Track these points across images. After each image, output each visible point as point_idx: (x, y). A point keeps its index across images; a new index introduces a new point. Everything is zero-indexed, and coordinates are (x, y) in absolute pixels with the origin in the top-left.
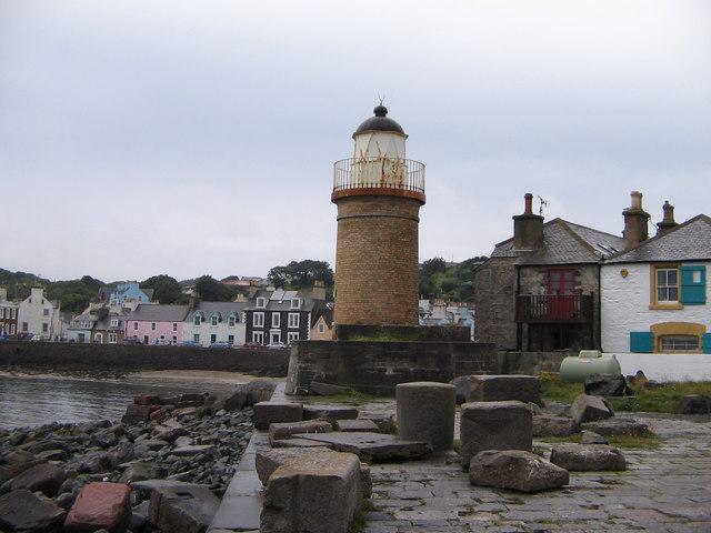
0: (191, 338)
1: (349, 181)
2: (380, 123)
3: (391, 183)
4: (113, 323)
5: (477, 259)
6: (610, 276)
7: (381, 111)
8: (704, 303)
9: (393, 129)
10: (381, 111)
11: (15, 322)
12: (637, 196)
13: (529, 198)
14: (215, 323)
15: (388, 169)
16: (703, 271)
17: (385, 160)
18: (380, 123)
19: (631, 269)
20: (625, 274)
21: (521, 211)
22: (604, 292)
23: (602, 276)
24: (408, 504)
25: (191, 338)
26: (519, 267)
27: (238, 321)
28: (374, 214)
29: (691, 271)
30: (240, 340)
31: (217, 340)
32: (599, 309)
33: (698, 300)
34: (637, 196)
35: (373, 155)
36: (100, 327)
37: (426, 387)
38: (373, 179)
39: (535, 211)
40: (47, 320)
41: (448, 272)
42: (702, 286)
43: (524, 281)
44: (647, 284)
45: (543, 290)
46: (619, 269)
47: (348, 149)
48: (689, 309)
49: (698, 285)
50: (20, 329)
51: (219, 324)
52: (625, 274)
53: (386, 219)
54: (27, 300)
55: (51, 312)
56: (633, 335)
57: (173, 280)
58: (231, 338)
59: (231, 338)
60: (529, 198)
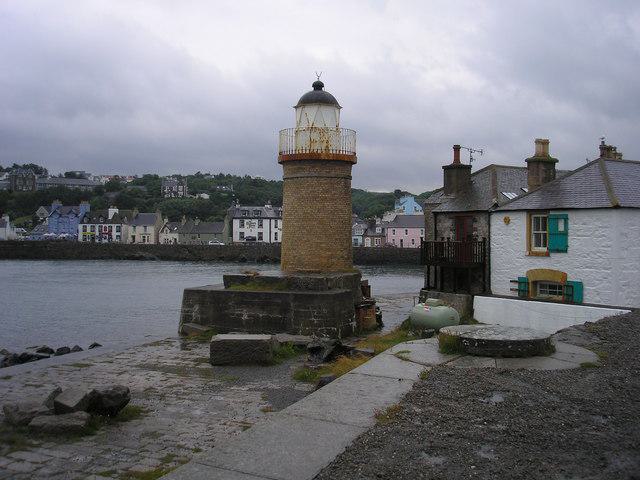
1: (293, 146)
2: (318, 97)
3: (318, 148)
4: (378, 230)
6: (497, 221)
7: (318, 86)
8: (566, 251)
10: (318, 86)
13: (457, 149)
16: (566, 220)
17: (312, 129)
18: (318, 97)
19: (512, 216)
21: (450, 160)
22: (493, 237)
23: (492, 224)
24: (209, 463)
28: (298, 175)
29: (557, 218)
35: (304, 126)
36: (370, 233)
39: (464, 160)
42: (565, 234)
44: (523, 231)
46: (502, 217)
47: (291, 118)
48: (555, 257)
49: (561, 234)
52: (507, 221)
60: (457, 149)
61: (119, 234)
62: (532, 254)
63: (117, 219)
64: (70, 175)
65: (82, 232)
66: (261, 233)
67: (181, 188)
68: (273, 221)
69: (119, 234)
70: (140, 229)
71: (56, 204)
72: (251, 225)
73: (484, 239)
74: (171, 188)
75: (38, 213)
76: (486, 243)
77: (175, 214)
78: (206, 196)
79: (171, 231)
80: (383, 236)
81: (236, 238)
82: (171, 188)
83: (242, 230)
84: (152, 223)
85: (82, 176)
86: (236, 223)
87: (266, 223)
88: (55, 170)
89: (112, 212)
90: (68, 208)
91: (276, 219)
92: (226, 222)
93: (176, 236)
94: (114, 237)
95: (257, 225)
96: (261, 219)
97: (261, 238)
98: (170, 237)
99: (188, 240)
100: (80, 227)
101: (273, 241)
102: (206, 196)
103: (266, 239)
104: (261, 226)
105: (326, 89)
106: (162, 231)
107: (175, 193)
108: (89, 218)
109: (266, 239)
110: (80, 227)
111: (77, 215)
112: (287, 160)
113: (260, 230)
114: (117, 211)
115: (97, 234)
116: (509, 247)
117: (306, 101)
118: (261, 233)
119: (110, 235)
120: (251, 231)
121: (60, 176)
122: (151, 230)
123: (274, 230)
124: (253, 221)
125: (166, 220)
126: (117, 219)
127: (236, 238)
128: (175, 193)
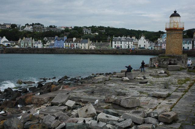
0: (187, 48)
1: (168, 27)
2: (175, 15)
3: (176, 27)
4: (159, 45)
7: (175, 12)
9: (178, 16)
10: (175, 12)
11: (137, 45)
12: (143, 61)
15: (175, 24)
18: (175, 15)
25: (187, 48)
27: (190, 43)
30: (191, 48)
34: (143, 61)
37: (171, 66)
38: (172, 27)
40: (145, 44)
50: (139, 46)
55: (146, 42)
58: (188, 47)
59: (188, 47)
61: (76, 46)
63: (76, 41)
64: (51, 27)
65: (66, 45)
66: (121, 46)
67: (89, 31)
68: (125, 42)
69: (76, 46)
70: (83, 44)
71: (56, 37)
72: (118, 43)
74: (86, 31)
75: (44, 39)
77: (94, 40)
78: (97, 34)
79: (93, 45)
80: (161, 47)
81: (113, 47)
82: (86, 31)
83: (115, 45)
84: (87, 43)
85: (55, 27)
86: (113, 42)
87: (123, 42)
88: (46, 25)
89: (74, 39)
90: (61, 38)
91: (126, 41)
92: (111, 42)
93: (95, 47)
94: (75, 47)
95: (120, 43)
96: (121, 41)
97: (121, 47)
98: (93, 47)
99: (98, 48)
100: (64, 44)
101: (125, 48)
102: (97, 34)
103: (123, 48)
104: (121, 43)
106: (90, 45)
107: (87, 33)
108: (67, 41)
109: (123, 48)
110: (64, 44)
111: (63, 40)
112: (167, 29)
113: (121, 45)
114: (75, 39)
115: (70, 46)
117: (172, 16)
118: (121, 46)
119: (74, 46)
120: (118, 44)
121: (48, 27)
122: (87, 45)
123: (125, 45)
124: (119, 42)
125: (91, 42)
126: (76, 41)
127: (113, 47)
128: (87, 33)
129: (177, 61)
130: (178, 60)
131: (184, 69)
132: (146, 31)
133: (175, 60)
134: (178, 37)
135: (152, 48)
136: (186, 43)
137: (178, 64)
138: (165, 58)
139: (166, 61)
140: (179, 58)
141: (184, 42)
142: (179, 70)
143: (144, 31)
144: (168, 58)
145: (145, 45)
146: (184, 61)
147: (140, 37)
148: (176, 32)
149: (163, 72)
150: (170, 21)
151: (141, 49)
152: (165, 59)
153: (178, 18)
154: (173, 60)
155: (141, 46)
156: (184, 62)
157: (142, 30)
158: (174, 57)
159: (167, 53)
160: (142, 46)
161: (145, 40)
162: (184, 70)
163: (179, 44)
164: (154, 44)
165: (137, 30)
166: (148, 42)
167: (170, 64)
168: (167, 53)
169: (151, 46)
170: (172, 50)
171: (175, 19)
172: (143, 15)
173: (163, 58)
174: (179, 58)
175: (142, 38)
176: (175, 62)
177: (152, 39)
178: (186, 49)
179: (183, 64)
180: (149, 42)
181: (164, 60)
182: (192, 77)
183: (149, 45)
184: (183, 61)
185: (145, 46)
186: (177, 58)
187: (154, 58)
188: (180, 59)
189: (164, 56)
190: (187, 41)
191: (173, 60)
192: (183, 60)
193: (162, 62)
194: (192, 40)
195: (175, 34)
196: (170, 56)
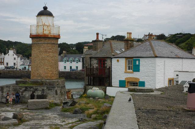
1: (34, 33)
2: (45, 12)
3: (46, 32)
5: (177, 34)
6: (114, 61)
7: (45, 8)
8: (139, 71)
9: (50, 14)
10: (45, 8)
11: (3, 62)
13: (98, 34)
14: (77, 62)
15: (45, 28)
16: (139, 61)
18: (45, 12)
19: (119, 59)
20: (118, 61)
21: (95, 39)
22: (113, 66)
26: (91, 58)
27: (79, 61)
29: (136, 60)
30: (80, 68)
31: (72, 68)
32: (111, 72)
33: (137, 70)
38: (40, 32)
40: (15, 61)
41: (166, 40)
42: (139, 66)
43: (92, 62)
45: (97, 65)
46: (116, 59)
48: (135, 73)
51: (73, 63)
52: (118, 61)
53: (44, 44)
54: (7, 54)
56: (120, 81)
57: (67, 44)
58: (77, 67)
59: (77, 67)
60: (98, 34)
62: (126, 72)
73: (109, 67)
76: (110, 70)
105: (48, 9)
116: (119, 70)
117: (41, 14)
129: (47, 91)
130: (49, 90)
131: (56, 105)
132: (20, 43)
133: (43, 90)
134: (50, 49)
135: (25, 67)
136: (73, 61)
137: (49, 96)
138: (26, 85)
139: (28, 91)
140: (51, 86)
141: (77, 59)
142: (47, 108)
143: (16, 43)
144: (32, 86)
145: (14, 64)
146: (58, 91)
147: (7, 51)
148: (47, 41)
149: (10, 115)
150: (37, 23)
151: (8, 70)
152: (26, 87)
153: (49, 18)
154: (41, 89)
155: (9, 65)
156: (59, 92)
157: (14, 41)
158: (42, 84)
159: (33, 78)
160: (11, 64)
161: (15, 56)
162: (56, 107)
163: (53, 62)
164: (27, 62)
165: (6, 40)
166: (19, 58)
167: (32, 97)
168: (33, 78)
169: (23, 65)
170: (41, 71)
171: (45, 19)
172: (12, 20)
173: (24, 85)
174: (50, 85)
175: (11, 52)
176: (44, 92)
177: (27, 54)
178: (73, 70)
179: (57, 96)
180: (21, 59)
181: (25, 90)
182: (64, 123)
183: (22, 63)
184: (56, 91)
185: (15, 65)
186: (47, 85)
187: (7, 87)
188: (52, 87)
189: (24, 83)
190: (75, 58)
191: (41, 89)
192: (56, 88)
193: (22, 92)
194: (82, 57)
195: (46, 45)
196: (36, 83)
